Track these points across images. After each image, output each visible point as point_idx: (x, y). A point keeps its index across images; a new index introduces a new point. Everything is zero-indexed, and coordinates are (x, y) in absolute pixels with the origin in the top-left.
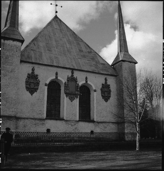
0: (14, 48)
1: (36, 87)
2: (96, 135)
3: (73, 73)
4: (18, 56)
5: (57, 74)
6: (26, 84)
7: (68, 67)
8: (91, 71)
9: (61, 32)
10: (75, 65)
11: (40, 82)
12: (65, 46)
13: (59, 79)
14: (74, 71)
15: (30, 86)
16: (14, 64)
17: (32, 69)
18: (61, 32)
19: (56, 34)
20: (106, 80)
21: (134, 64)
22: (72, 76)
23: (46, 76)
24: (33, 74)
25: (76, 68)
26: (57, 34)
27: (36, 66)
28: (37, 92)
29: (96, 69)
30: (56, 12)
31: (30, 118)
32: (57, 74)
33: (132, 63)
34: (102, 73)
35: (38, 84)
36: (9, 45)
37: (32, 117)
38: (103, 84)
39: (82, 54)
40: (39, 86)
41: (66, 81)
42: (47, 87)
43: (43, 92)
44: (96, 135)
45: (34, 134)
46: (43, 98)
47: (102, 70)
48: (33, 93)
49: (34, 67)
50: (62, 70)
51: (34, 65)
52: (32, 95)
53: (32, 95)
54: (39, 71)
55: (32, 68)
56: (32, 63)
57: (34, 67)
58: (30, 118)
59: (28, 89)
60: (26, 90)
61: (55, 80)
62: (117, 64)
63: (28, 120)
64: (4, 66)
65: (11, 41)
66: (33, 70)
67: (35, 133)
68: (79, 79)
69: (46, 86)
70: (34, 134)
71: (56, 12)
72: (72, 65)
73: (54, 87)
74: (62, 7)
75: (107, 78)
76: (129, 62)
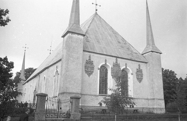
0: (79, 40)
1: (92, 71)
2: (92, 108)
3: (117, 60)
4: (81, 46)
5: (106, 61)
6: (85, 68)
7: (113, 55)
8: (129, 58)
9: (103, 26)
10: (118, 54)
11: (94, 66)
12: (108, 38)
13: (107, 65)
14: (118, 59)
15: (88, 70)
16: (79, 53)
17: (89, 56)
18: (103, 26)
19: (99, 28)
20: (139, 65)
21: (159, 54)
22: (116, 62)
23: (98, 62)
24: (90, 60)
25: (120, 57)
26: (100, 29)
27: (92, 54)
28: (93, 74)
29: (132, 58)
30: (97, 10)
31: (88, 95)
32: (106, 61)
33: (158, 54)
34: (137, 60)
35: (93, 68)
36: (75, 38)
37: (90, 94)
38: (137, 69)
39: (120, 45)
40: (94, 69)
41: (112, 66)
42: (99, 70)
43: (97, 75)
44: (92, 108)
45: (84, 107)
46: (97, 79)
47: (137, 58)
48: (90, 75)
49: (90, 55)
50: (109, 57)
51: (90, 54)
52: (89, 76)
53: (89, 76)
54: (95, 58)
55: (89, 55)
56: (89, 52)
57: (90, 55)
58: (88, 95)
59: (86, 72)
60: (85, 73)
61: (104, 65)
62: (147, 54)
63: (87, 96)
64: (72, 54)
65: (77, 35)
66: (90, 57)
67: (92, 107)
68: (121, 65)
69: (98, 70)
70: (84, 107)
71: (97, 10)
72: (116, 54)
73: (104, 70)
74: (100, 6)
75: (91, 56)
76: (156, 52)
